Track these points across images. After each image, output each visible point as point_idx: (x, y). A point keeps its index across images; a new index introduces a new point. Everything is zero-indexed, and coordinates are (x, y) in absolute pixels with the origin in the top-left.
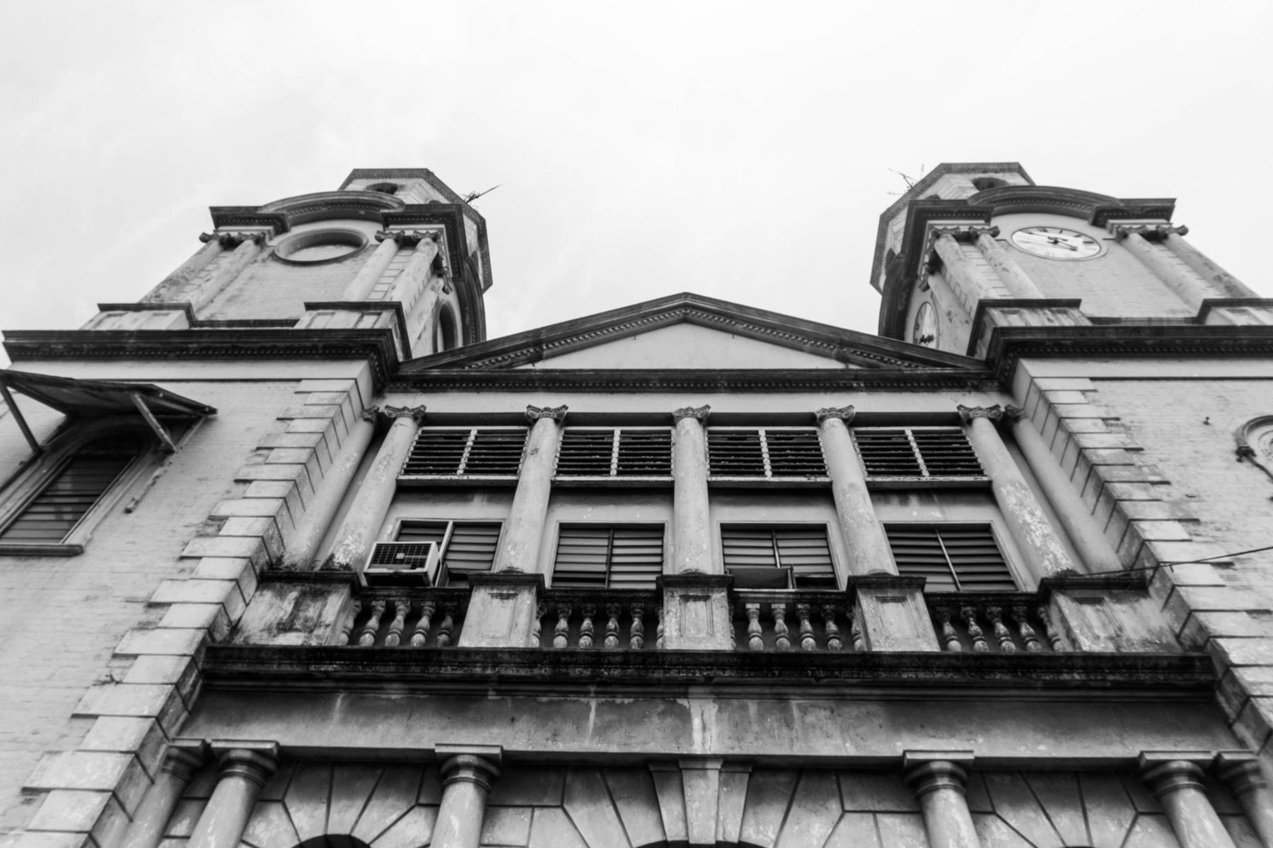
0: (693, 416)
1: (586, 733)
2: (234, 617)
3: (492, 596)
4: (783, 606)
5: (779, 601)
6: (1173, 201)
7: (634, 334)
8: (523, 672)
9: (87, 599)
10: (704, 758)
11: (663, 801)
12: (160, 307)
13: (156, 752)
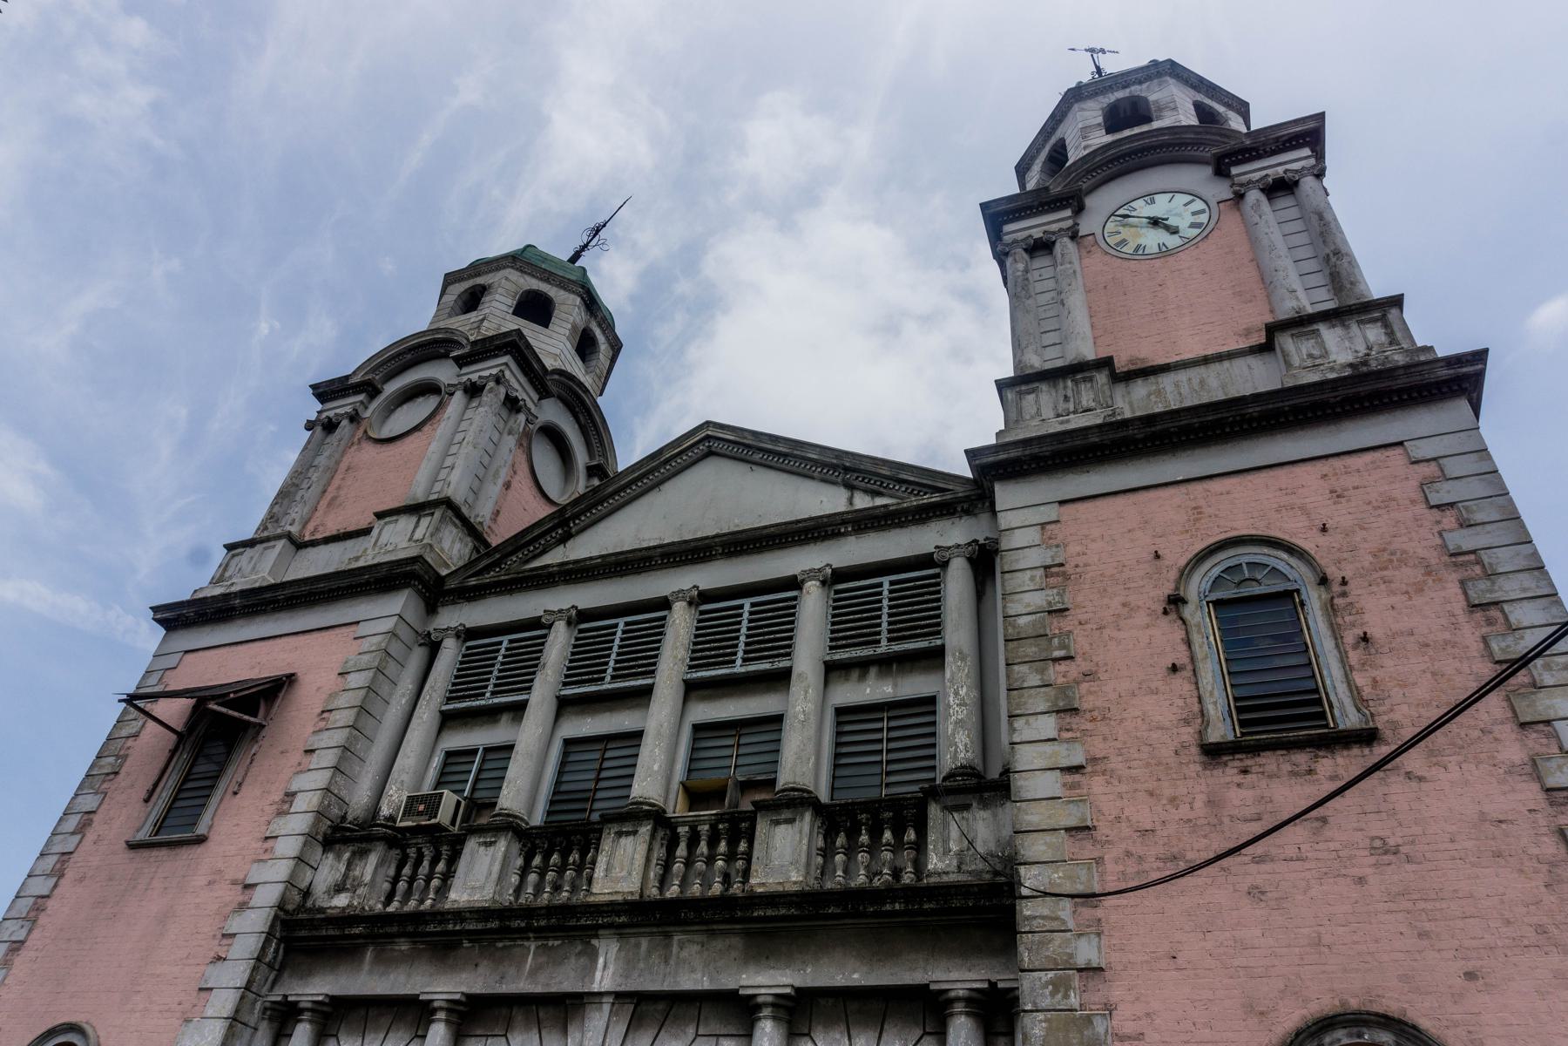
0: (683, 599)
1: (526, 975)
2: (303, 885)
3: (480, 844)
4: (707, 827)
5: (704, 822)
6: (1321, 117)
7: (657, 485)
8: (480, 926)
9: (210, 883)
10: (600, 994)
11: (570, 1029)
12: (268, 539)
13: (253, 1008)
